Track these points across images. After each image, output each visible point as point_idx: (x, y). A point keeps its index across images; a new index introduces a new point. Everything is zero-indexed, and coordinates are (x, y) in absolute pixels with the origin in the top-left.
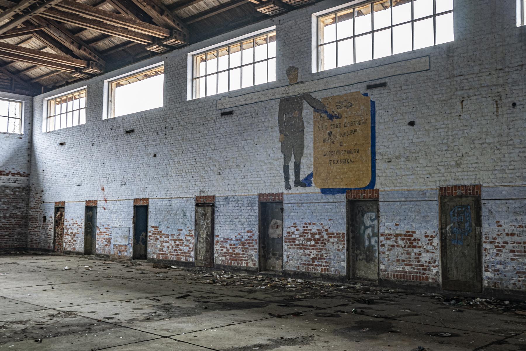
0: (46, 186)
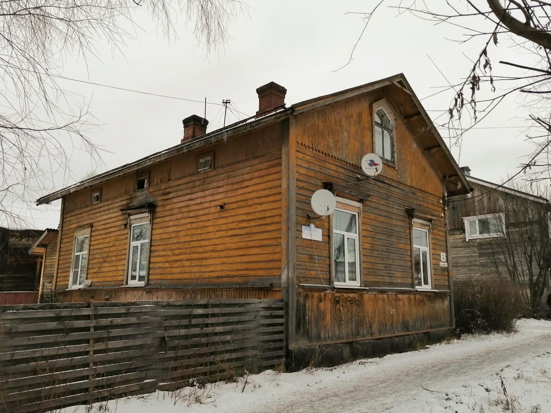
0: (482, 336)
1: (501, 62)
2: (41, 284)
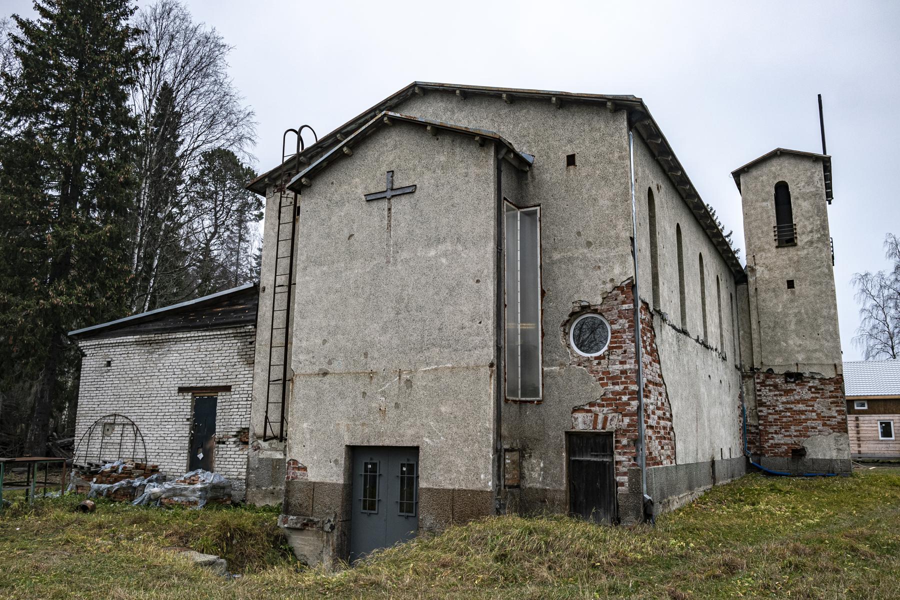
0: (413, 133)
1: (819, 96)
2: (374, 120)
